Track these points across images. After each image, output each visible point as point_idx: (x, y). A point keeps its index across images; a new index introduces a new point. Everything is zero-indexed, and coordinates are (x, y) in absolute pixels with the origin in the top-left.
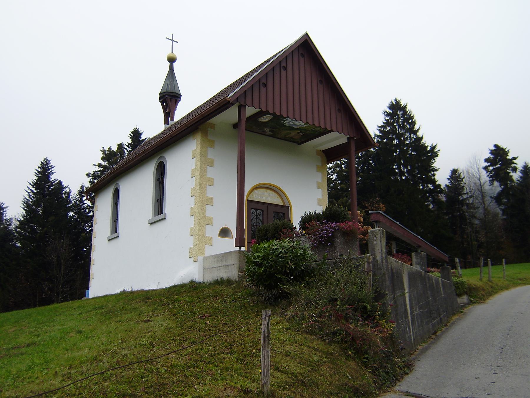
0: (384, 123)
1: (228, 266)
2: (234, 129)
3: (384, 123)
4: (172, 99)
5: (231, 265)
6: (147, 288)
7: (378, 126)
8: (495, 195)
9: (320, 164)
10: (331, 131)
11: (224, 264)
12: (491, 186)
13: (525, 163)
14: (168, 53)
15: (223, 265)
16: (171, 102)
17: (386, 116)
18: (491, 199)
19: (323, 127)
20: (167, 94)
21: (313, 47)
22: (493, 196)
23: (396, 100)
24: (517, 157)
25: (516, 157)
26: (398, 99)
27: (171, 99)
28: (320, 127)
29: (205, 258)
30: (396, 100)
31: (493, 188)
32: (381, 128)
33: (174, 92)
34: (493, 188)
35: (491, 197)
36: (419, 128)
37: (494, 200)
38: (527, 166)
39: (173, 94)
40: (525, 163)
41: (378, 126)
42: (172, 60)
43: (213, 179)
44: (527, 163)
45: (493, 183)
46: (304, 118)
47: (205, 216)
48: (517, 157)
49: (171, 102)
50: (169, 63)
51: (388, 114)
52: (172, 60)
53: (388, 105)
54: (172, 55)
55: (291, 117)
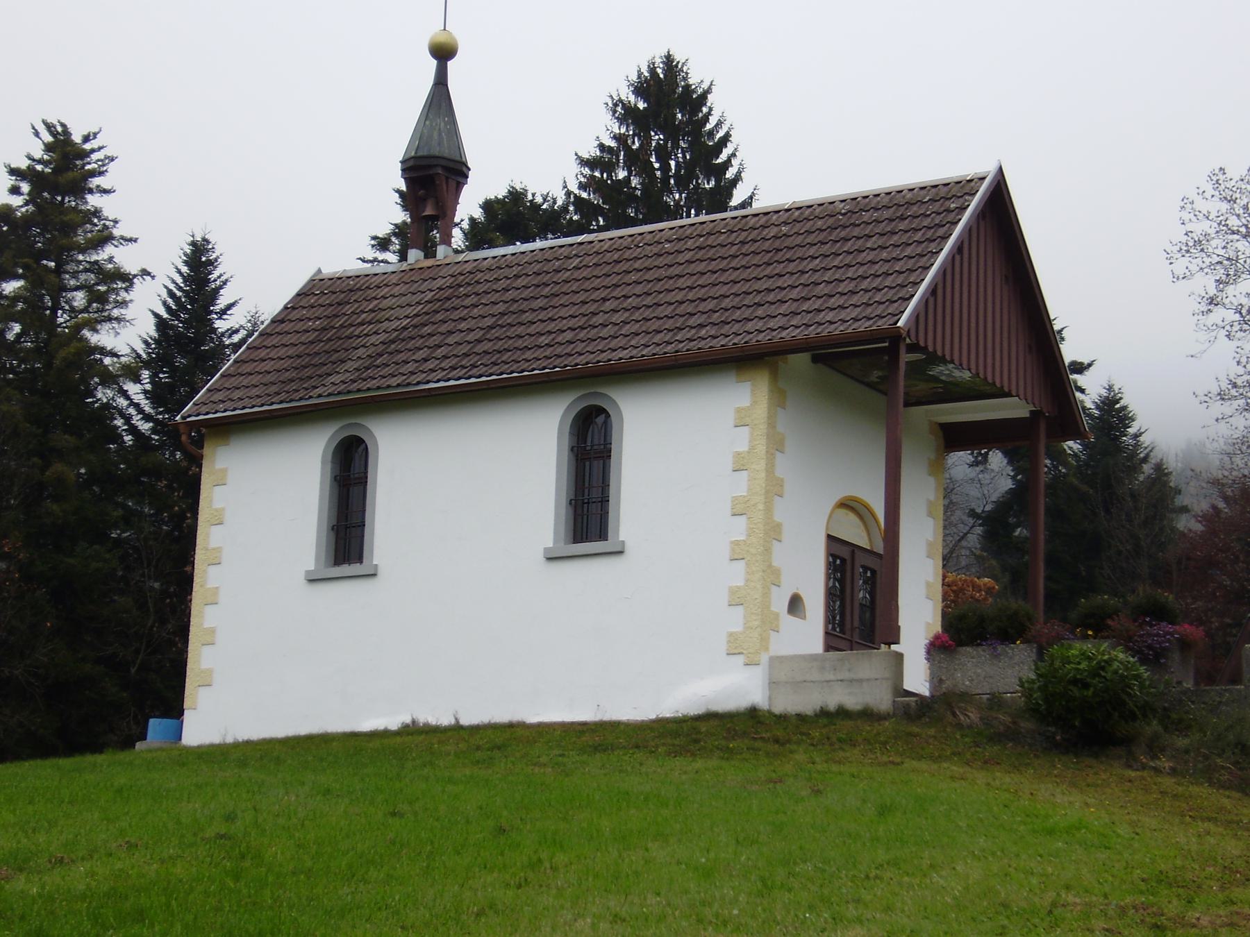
0: (602, 147)
1: (860, 681)
2: (812, 365)
3: (602, 147)
4: (450, 180)
5: (868, 680)
6: (533, 719)
7: (579, 157)
8: (988, 508)
9: (933, 457)
10: (1009, 395)
11: (846, 675)
12: (978, 469)
13: (1110, 388)
14: (430, 31)
15: (842, 678)
16: (447, 187)
17: (622, 120)
18: (971, 521)
19: (998, 385)
20: (443, 163)
21: (1007, 200)
22: (979, 510)
23: (669, 59)
24: (1090, 365)
25: (1086, 360)
26: (679, 57)
27: (447, 178)
28: (994, 383)
29: (773, 660)
30: (669, 59)
31: (985, 478)
32: (592, 170)
33: (458, 159)
34: (985, 478)
35: (973, 513)
36: (751, 198)
37: (980, 525)
38: (1117, 402)
39: (451, 165)
40: (1110, 388)
41: (579, 157)
42: (443, 53)
43: (782, 480)
44: (1116, 389)
45: (987, 453)
46: (973, 366)
47: (770, 566)
48: (1090, 365)
49: (447, 187)
50: (435, 62)
51: (627, 114)
52: (443, 53)
53: (634, 77)
54: (442, 38)
55: (957, 362)
